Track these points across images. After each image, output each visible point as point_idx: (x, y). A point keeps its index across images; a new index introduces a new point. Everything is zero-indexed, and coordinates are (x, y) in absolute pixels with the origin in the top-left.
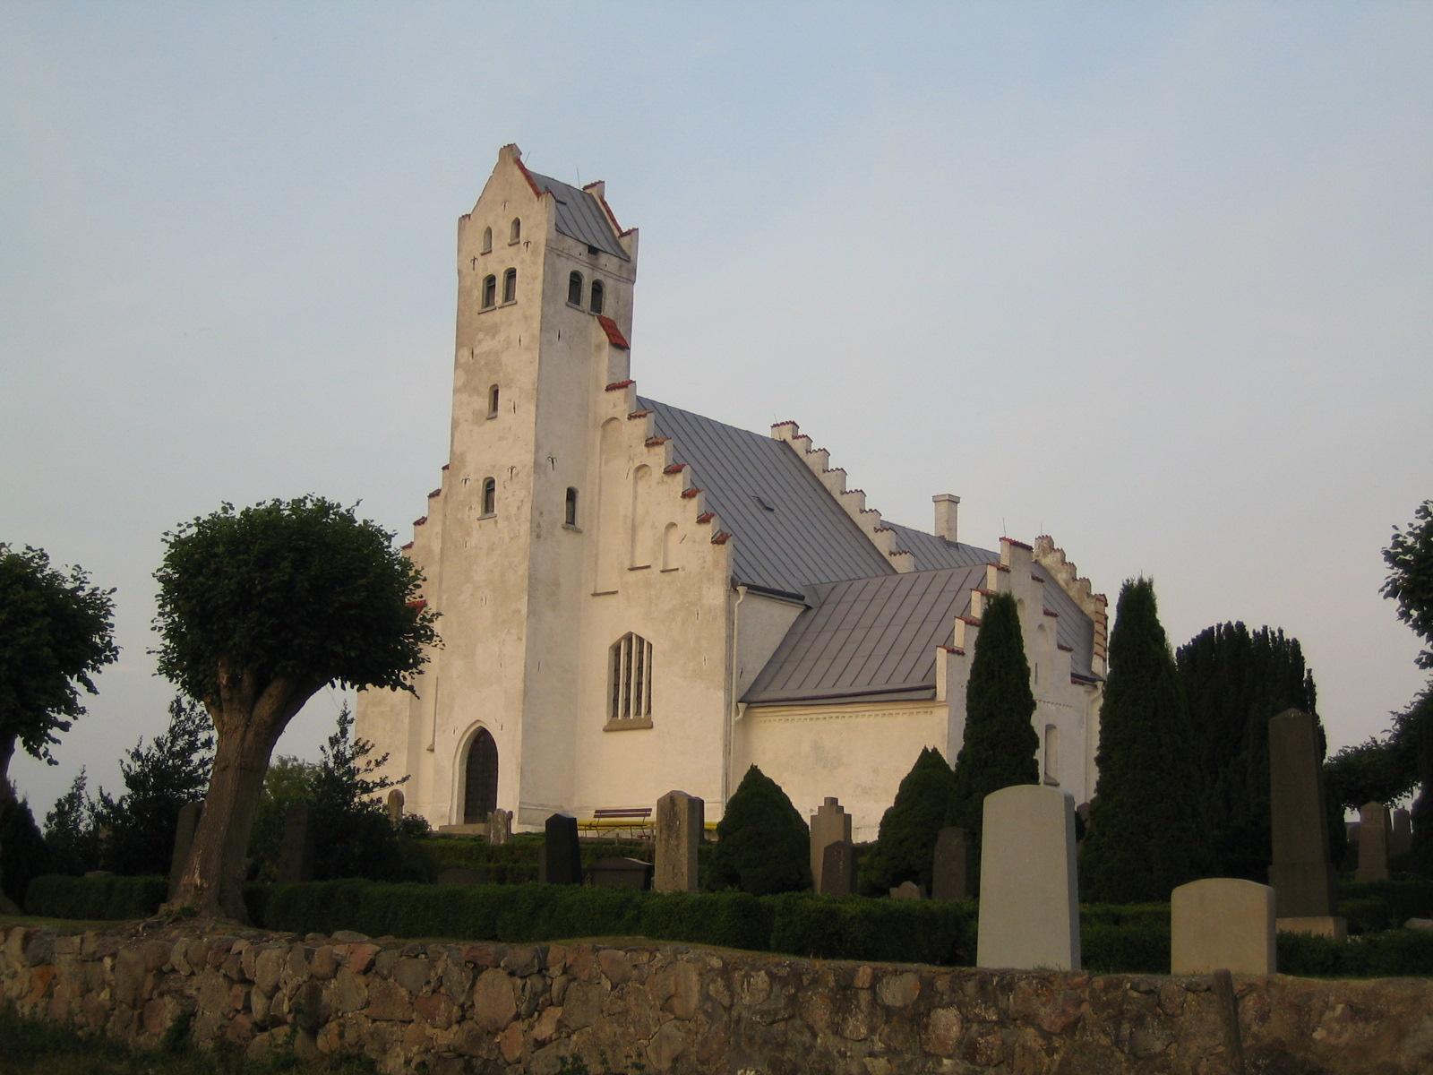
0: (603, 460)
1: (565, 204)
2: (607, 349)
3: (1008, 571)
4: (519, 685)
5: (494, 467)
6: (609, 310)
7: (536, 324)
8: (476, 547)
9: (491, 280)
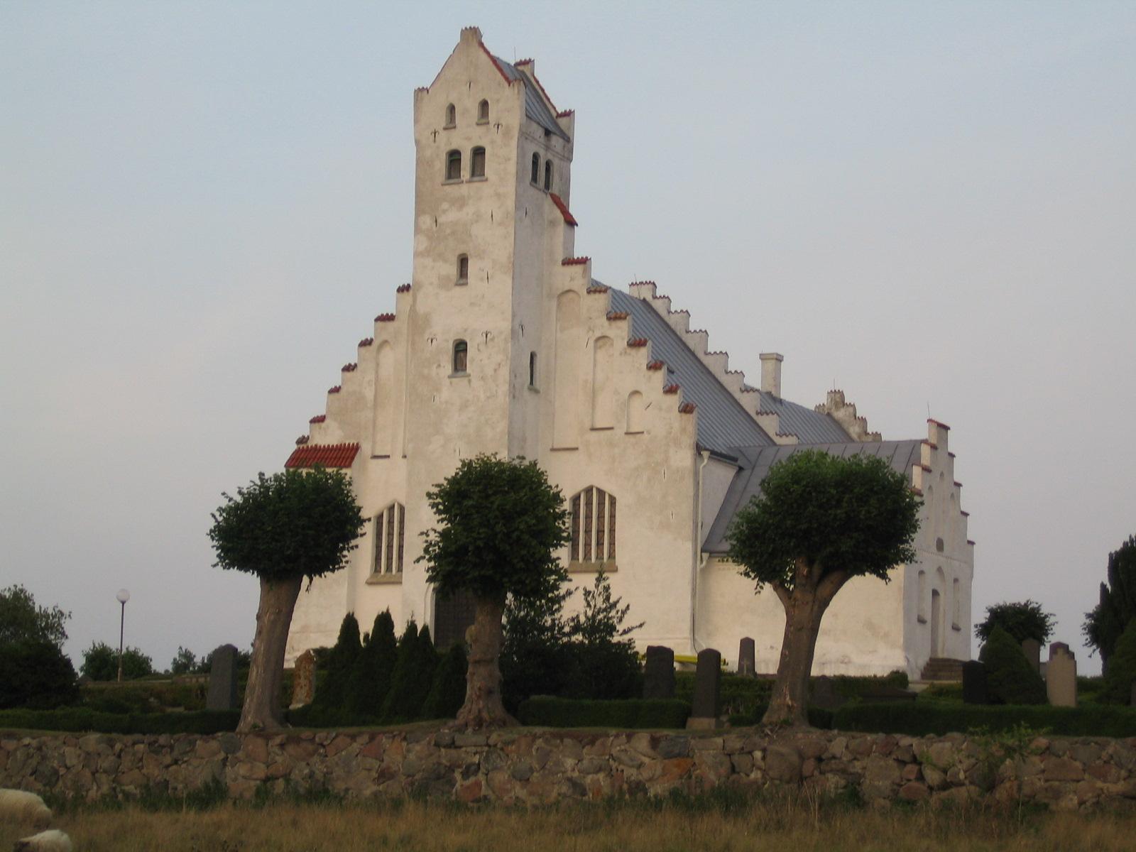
5: (466, 330)
6: (555, 189)
8: (446, 402)
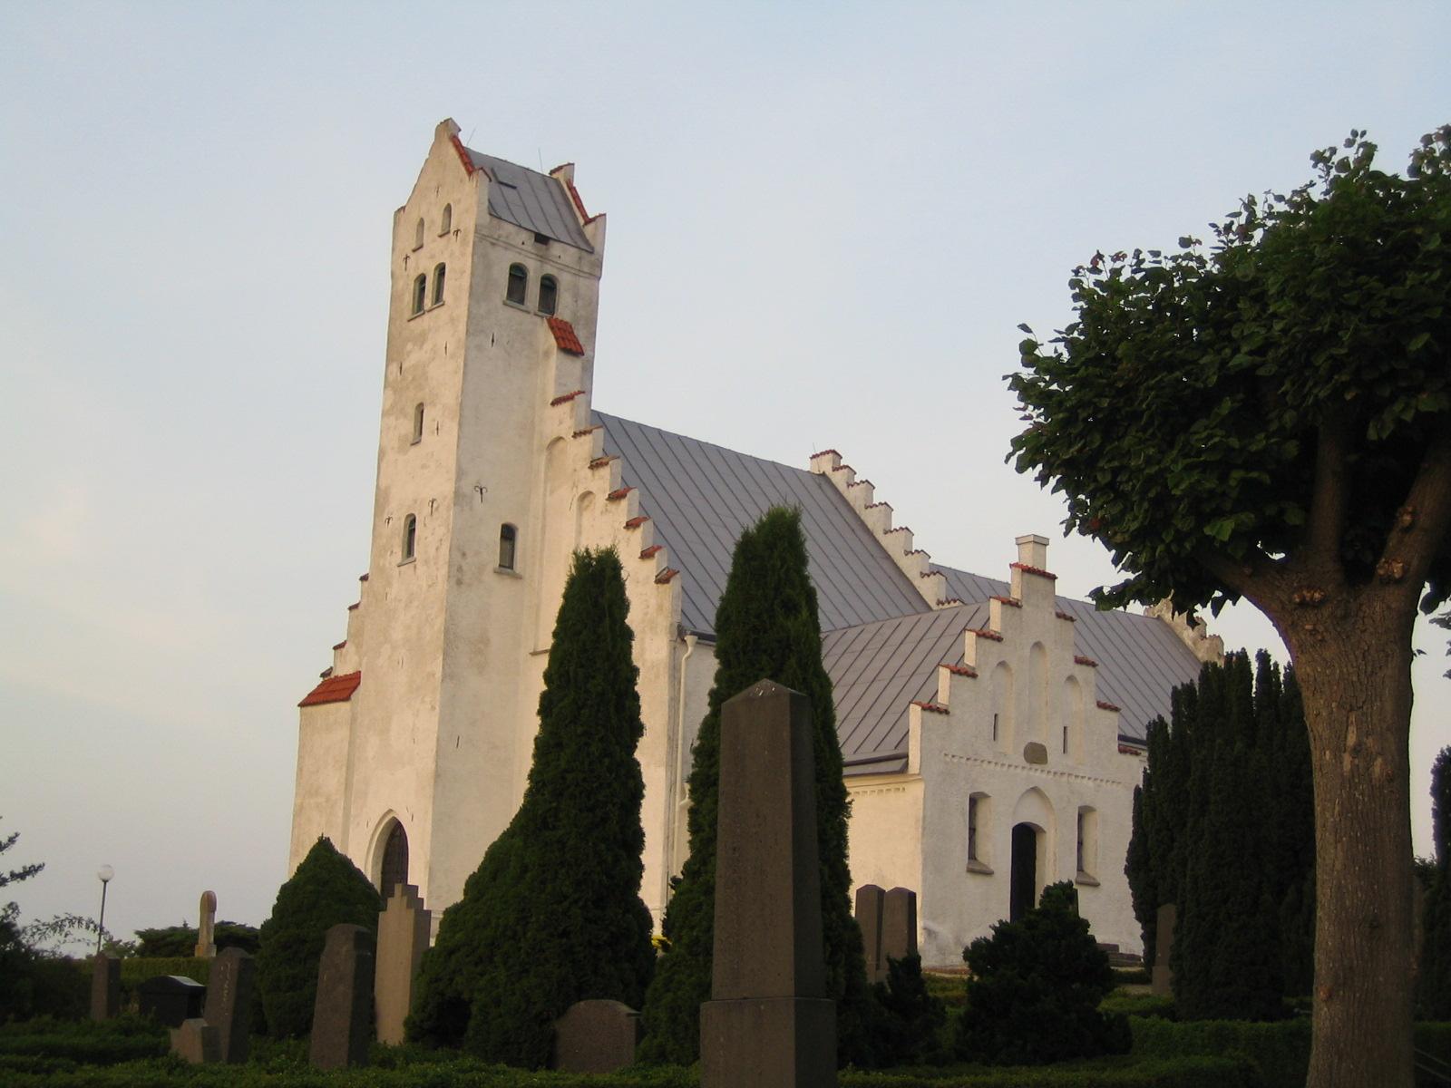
0: (548, 489)
1: (514, 188)
2: (556, 357)
3: (1019, 607)
4: (431, 766)
6: (565, 310)
7: (462, 328)
9: (422, 280)
